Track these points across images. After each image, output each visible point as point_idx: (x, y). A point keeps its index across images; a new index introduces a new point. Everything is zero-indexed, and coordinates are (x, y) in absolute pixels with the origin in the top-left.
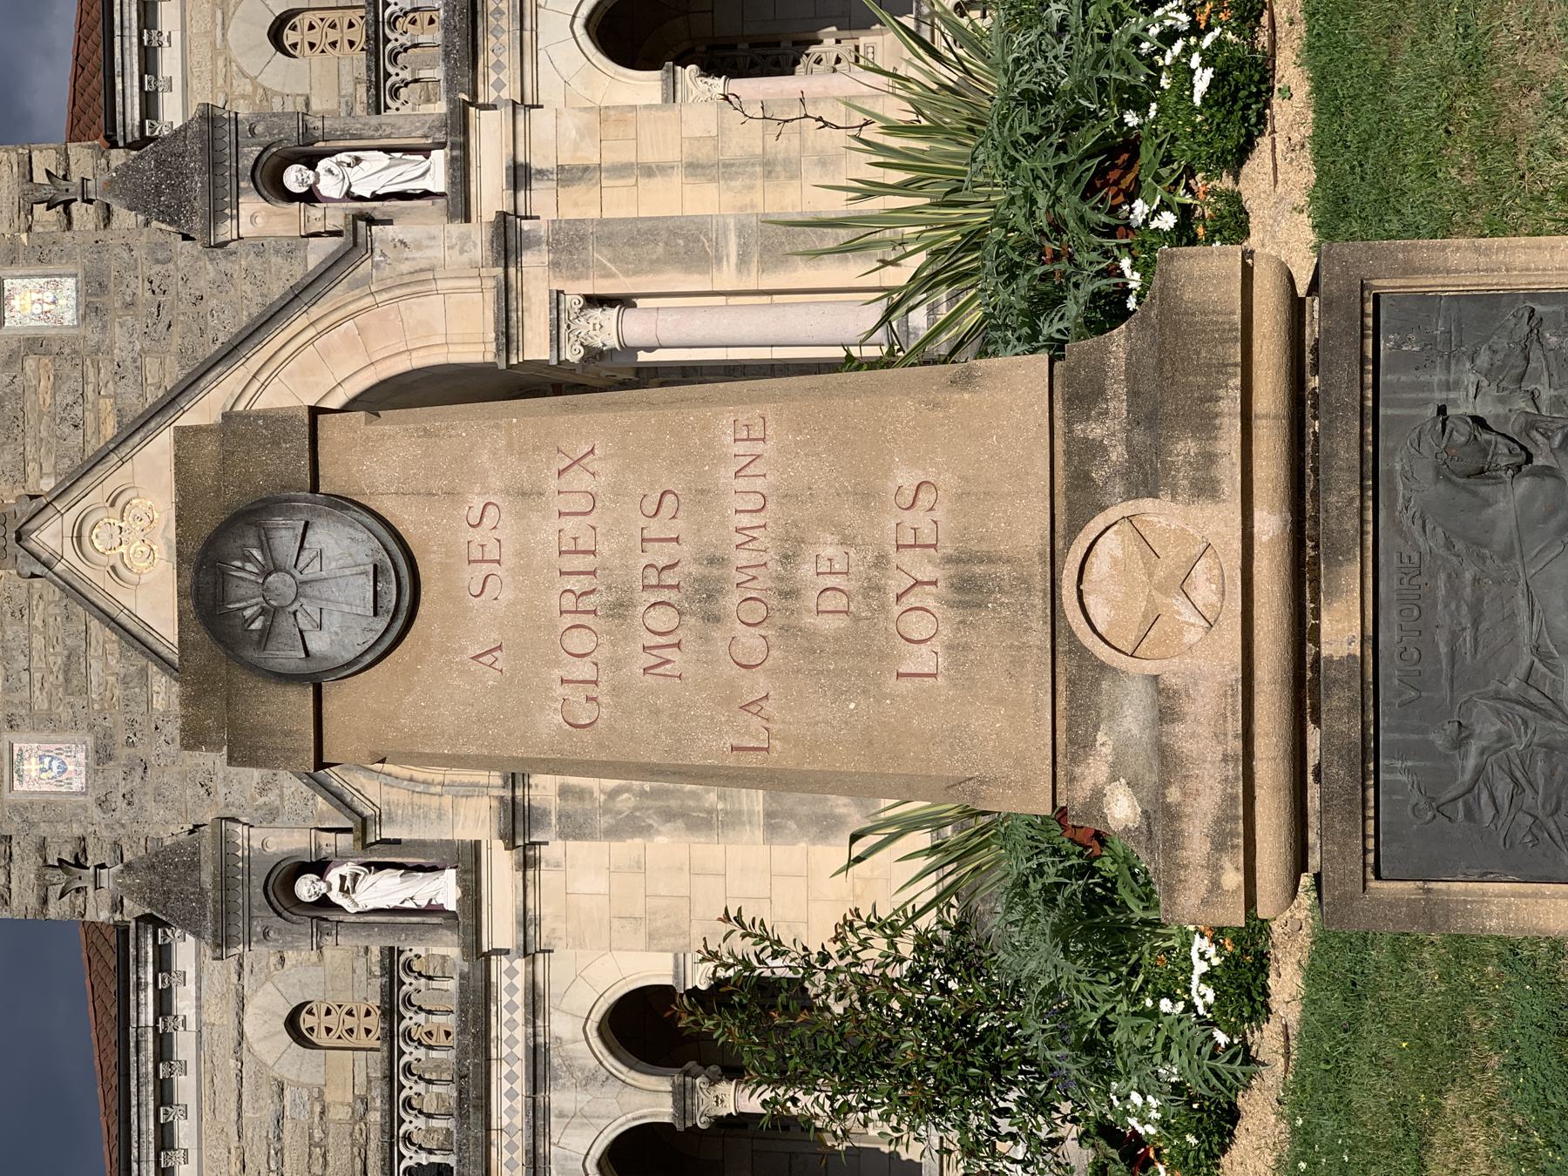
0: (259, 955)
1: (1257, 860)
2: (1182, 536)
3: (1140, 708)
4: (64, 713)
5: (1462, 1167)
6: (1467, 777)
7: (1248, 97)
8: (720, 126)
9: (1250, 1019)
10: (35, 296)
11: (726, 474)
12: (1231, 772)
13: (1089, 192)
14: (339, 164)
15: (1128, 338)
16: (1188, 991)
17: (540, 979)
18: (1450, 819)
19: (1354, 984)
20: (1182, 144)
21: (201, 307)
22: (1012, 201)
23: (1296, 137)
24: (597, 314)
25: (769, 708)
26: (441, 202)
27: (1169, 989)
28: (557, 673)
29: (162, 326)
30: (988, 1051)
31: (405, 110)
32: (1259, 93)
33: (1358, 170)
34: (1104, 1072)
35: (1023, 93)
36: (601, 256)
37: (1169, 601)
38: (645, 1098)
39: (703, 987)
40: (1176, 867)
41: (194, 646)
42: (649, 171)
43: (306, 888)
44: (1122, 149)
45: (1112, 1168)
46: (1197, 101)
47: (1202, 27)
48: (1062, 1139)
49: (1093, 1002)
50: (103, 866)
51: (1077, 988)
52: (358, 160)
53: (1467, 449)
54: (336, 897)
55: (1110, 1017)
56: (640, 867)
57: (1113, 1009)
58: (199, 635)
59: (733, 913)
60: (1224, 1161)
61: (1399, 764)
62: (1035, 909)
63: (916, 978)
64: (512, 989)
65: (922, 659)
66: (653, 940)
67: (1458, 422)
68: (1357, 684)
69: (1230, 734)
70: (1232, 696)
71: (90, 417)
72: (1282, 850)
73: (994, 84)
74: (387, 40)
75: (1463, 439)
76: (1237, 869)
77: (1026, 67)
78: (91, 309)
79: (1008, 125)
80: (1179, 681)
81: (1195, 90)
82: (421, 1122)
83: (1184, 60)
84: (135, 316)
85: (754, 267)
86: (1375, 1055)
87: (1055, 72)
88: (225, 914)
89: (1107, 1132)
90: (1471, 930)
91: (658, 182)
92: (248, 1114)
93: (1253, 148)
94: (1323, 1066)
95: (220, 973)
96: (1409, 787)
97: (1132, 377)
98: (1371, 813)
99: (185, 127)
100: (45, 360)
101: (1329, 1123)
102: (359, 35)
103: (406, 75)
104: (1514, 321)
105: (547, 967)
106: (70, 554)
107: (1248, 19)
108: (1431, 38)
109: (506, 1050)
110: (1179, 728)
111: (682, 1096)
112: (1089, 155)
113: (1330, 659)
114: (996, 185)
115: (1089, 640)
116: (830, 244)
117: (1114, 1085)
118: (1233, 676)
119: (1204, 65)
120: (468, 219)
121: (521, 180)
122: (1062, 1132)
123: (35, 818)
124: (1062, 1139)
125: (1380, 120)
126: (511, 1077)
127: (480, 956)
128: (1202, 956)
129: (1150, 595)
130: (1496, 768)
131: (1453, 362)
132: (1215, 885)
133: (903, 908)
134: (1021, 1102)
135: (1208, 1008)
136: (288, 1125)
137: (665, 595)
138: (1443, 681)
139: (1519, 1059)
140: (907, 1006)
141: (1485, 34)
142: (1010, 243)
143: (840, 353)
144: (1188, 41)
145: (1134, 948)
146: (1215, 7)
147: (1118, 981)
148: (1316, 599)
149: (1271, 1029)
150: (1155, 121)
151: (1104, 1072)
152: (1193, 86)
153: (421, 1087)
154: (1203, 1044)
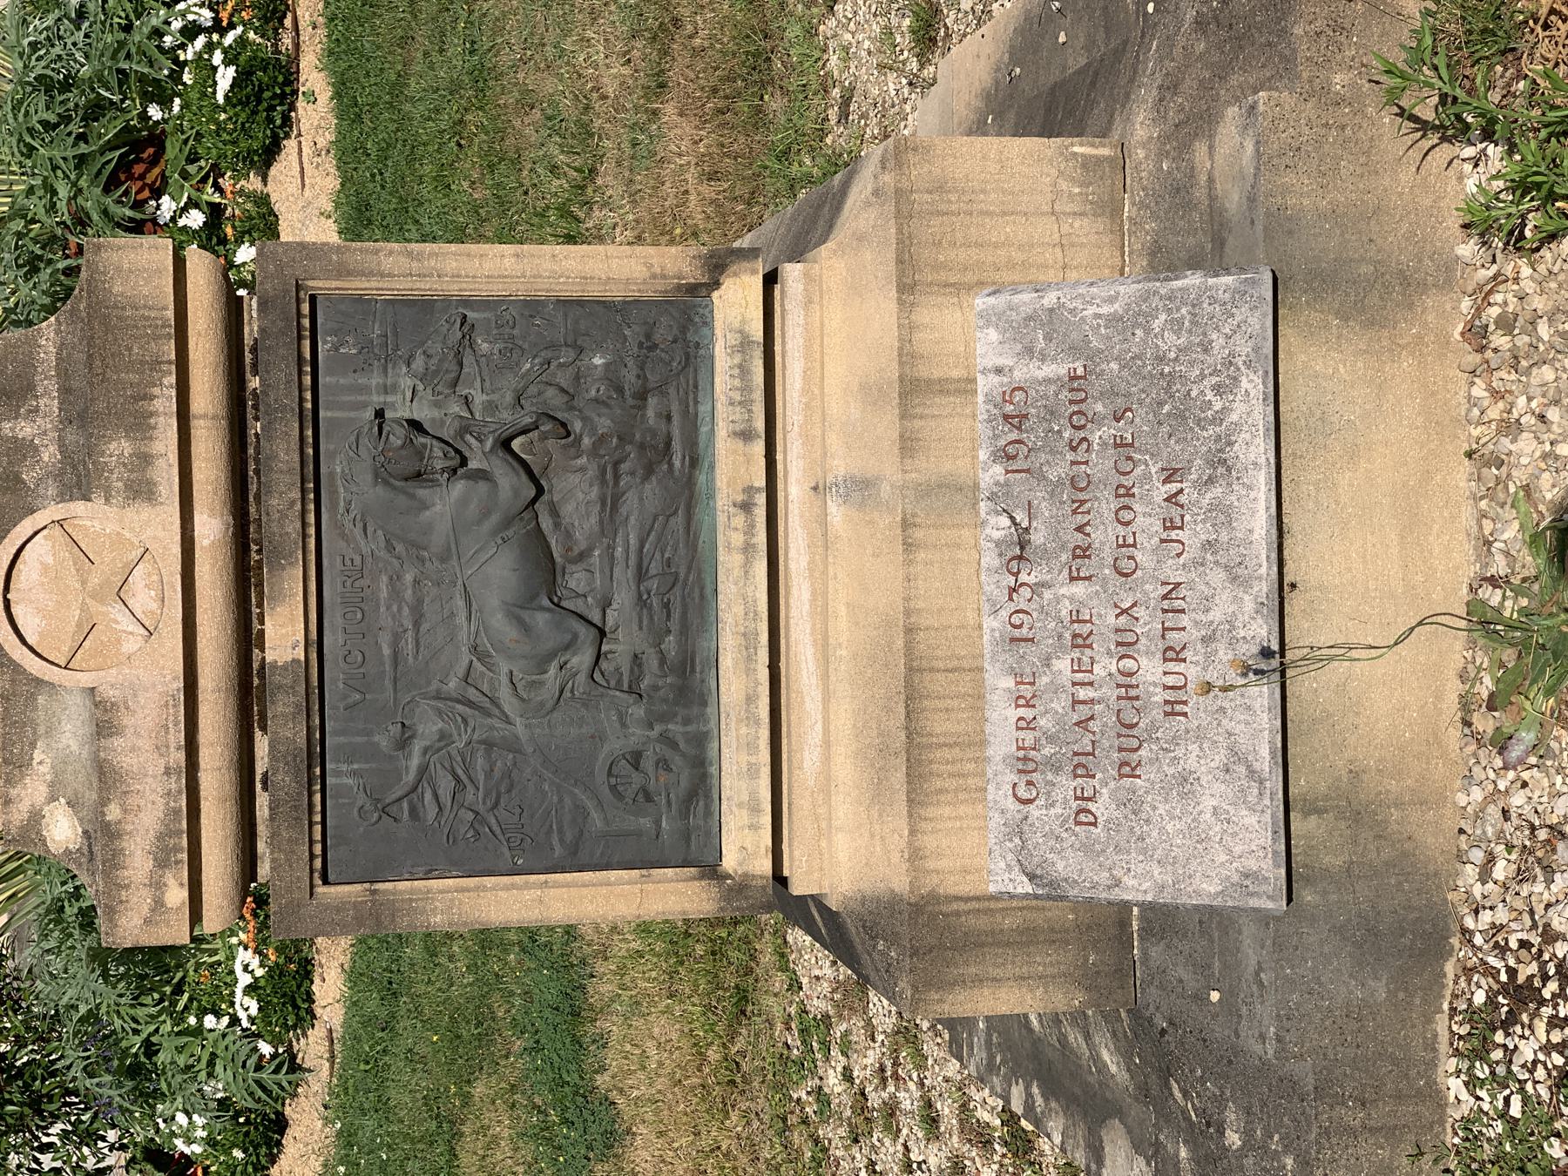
1: (204, 874)
3: (79, 723)
5: (489, 1152)
6: (410, 777)
7: (271, 98)
9: (295, 1027)
12: (174, 786)
15: (58, 332)
16: (232, 1004)
18: (395, 820)
19: (390, 983)
22: (30, 191)
23: (322, 143)
27: (214, 1004)
30: (27, 1086)
32: (283, 96)
33: (378, 178)
34: (148, 1095)
35: (39, 78)
37: (104, 609)
40: (115, 886)
46: (220, 99)
47: (224, 24)
49: (134, 1026)
51: (118, 1013)
53: (404, 452)
55: (153, 1039)
57: (157, 1030)
61: (344, 767)
62: (71, 935)
67: (394, 425)
68: (302, 689)
69: (173, 746)
70: (174, 706)
72: (229, 862)
75: (399, 442)
76: (182, 885)
77: (42, 52)
79: (23, 110)
80: (117, 693)
81: (218, 88)
83: (206, 56)
86: (410, 1050)
87: (75, 61)
90: (416, 927)
93: (280, 150)
94: (362, 1067)
96: (355, 789)
97: (63, 373)
98: (318, 818)
104: (447, 326)
107: (271, 19)
108: (441, 51)
110: (117, 742)
112: (111, 146)
113: (274, 665)
114: (13, 173)
117: (160, 1107)
118: (175, 686)
122: (108, 1162)
125: (398, 130)
128: (246, 968)
129: (83, 602)
130: (438, 766)
131: (390, 366)
132: (159, 903)
134: (65, 1135)
135: (252, 1020)
138: (387, 682)
139: (537, 1042)
141: (490, 50)
142: (32, 235)
144: (210, 38)
145: (179, 966)
146: (237, 5)
147: (161, 1001)
148: (260, 605)
150: (181, 117)
151: (148, 1095)
152: (215, 83)
154: (249, 1057)
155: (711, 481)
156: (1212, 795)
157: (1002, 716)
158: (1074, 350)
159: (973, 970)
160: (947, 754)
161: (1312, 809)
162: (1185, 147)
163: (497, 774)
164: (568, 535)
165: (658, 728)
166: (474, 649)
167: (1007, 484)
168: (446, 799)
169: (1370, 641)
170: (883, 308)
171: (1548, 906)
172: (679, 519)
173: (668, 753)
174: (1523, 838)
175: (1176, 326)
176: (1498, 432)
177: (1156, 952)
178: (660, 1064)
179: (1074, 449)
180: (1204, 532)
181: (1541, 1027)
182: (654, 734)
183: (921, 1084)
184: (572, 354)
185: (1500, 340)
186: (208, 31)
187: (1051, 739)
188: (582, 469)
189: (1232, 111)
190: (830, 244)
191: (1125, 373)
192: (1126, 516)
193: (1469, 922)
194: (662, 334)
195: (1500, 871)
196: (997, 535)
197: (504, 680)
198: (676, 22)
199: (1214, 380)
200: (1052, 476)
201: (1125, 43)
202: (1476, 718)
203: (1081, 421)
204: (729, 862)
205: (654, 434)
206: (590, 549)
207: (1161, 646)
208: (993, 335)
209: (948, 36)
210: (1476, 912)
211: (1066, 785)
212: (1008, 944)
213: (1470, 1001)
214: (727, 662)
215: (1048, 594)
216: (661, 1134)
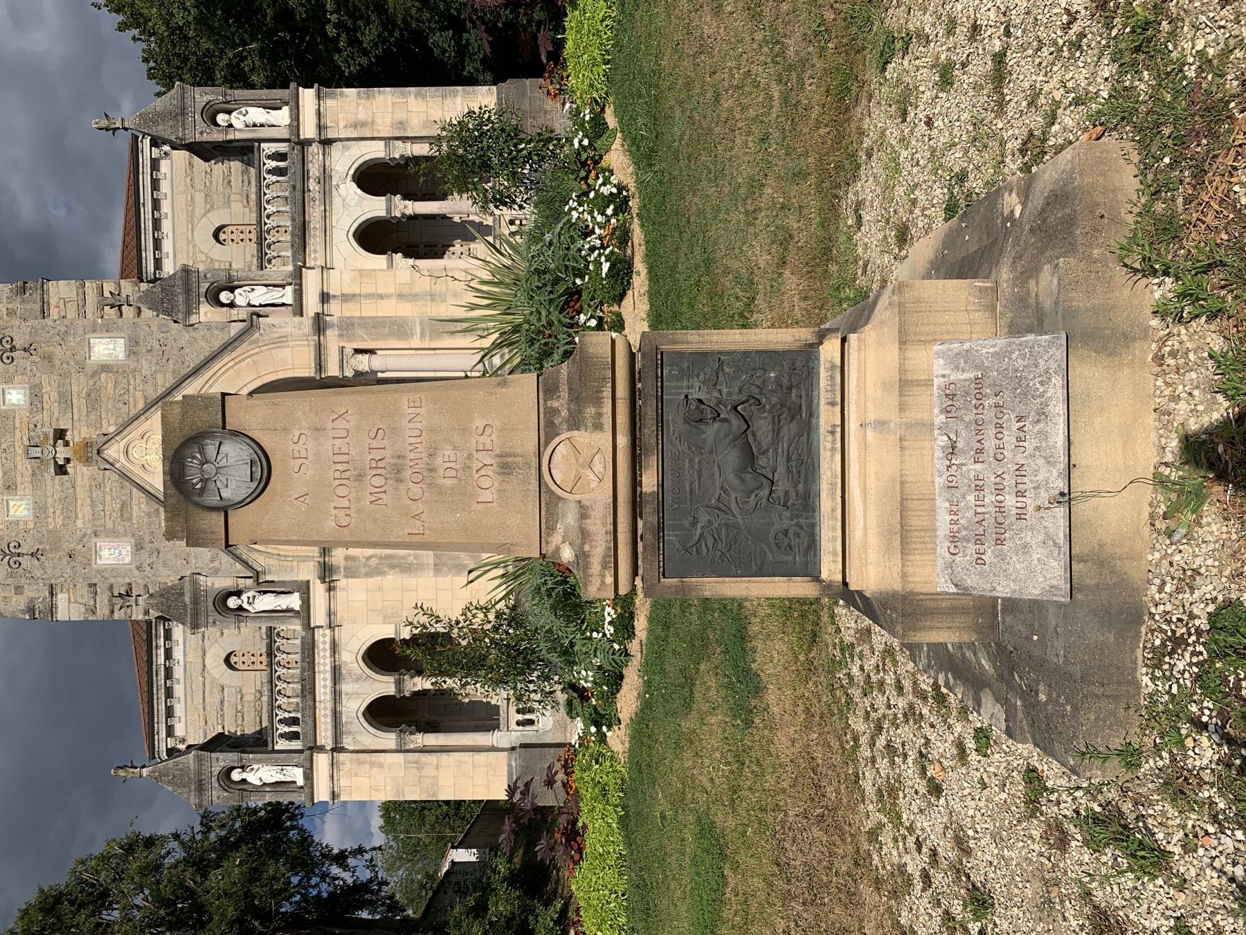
0: (212, 632)
2: (589, 446)
4: (120, 529)
8: (412, 279)
10: (105, 347)
11: (405, 422)
13: (562, 310)
17: (336, 637)
20: (598, 292)
21: (183, 351)
22: (531, 313)
23: (642, 291)
24: (360, 356)
25: (424, 517)
26: (290, 308)
28: (333, 504)
29: (164, 360)
31: (274, 269)
35: (535, 269)
36: (361, 332)
38: (382, 685)
40: (587, 575)
41: (171, 496)
42: (381, 297)
43: (232, 602)
44: (574, 294)
45: (574, 701)
46: (604, 276)
48: (555, 691)
50: (139, 596)
52: (253, 290)
54: (245, 606)
56: (380, 589)
58: (172, 491)
59: (419, 605)
60: (618, 696)
63: (496, 629)
64: (324, 642)
65: (487, 496)
66: (386, 620)
71: (131, 400)
73: (524, 265)
74: (266, 239)
78: (132, 352)
82: (285, 700)
84: (152, 356)
85: (427, 338)
88: (196, 614)
89: (573, 687)
91: (385, 301)
95: (194, 640)
97: (569, 383)
99: (175, 274)
100: (110, 375)
101: (657, 678)
102: (253, 236)
103: (275, 254)
105: (340, 632)
106: (123, 459)
109: (322, 668)
110: (588, 521)
111: (399, 684)
112: (562, 295)
113: (646, 493)
115: (554, 487)
116: (460, 329)
119: (606, 261)
120: (302, 316)
121: (325, 299)
124: (555, 691)
126: (324, 679)
127: (309, 629)
132: (603, 583)
133: (490, 601)
134: (538, 677)
135: (611, 635)
136: (226, 704)
137: (379, 471)
140: (492, 640)
143: (463, 374)
148: (640, 470)
149: (635, 642)
153: (285, 685)
155: (818, 422)
156: (1037, 553)
157: (943, 520)
158: (977, 367)
159: (928, 623)
160: (917, 534)
161: (1082, 560)
162: (1025, 282)
163: (730, 537)
164: (760, 444)
165: (795, 521)
166: (722, 488)
167: (947, 423)
168: (710, 546)
169: (1109, 489)
170: (892, 352)
171: (1191, 604)
172: (805, 436)
173: (799, 531)
174: (1179, 574)
175: (1023, 357)
176: (1169, 400)
177: (1008, 619)
178: (779, 660)
179: (977, 408)
180: (1035, 443)
181: (1187, 655)
182: (793, 523)
183: (895, 673)
184: (762, 372)
185: (1171, 361)
186: (599, 249)
187: (966, 529)
188: (765, 418)
189: (1047, 267)
190: (869, 326)
191: (1000, 377)
192: (1000, 436)
193: (1153, 610)
194: (798, 364)
195: (1168, 588)
196: (942, 444)
197: (733, 500)
198: (791, 236)
199: (1040, 379)
200: (967, 419)
201: (996, 239)
202: (1157, 523)
203: (980, 396)
204: (824, 576)
205: (795, 404)
206: (769, 449)
207: (1015, 490)
208: (941, 361)
209: (912, 238)
210: (1156, 605)
211: (972, 548)
212: (944, 614)
213: (1153, 644)
214: (823, 495)
215: (964, 468)
216: (779, 689)
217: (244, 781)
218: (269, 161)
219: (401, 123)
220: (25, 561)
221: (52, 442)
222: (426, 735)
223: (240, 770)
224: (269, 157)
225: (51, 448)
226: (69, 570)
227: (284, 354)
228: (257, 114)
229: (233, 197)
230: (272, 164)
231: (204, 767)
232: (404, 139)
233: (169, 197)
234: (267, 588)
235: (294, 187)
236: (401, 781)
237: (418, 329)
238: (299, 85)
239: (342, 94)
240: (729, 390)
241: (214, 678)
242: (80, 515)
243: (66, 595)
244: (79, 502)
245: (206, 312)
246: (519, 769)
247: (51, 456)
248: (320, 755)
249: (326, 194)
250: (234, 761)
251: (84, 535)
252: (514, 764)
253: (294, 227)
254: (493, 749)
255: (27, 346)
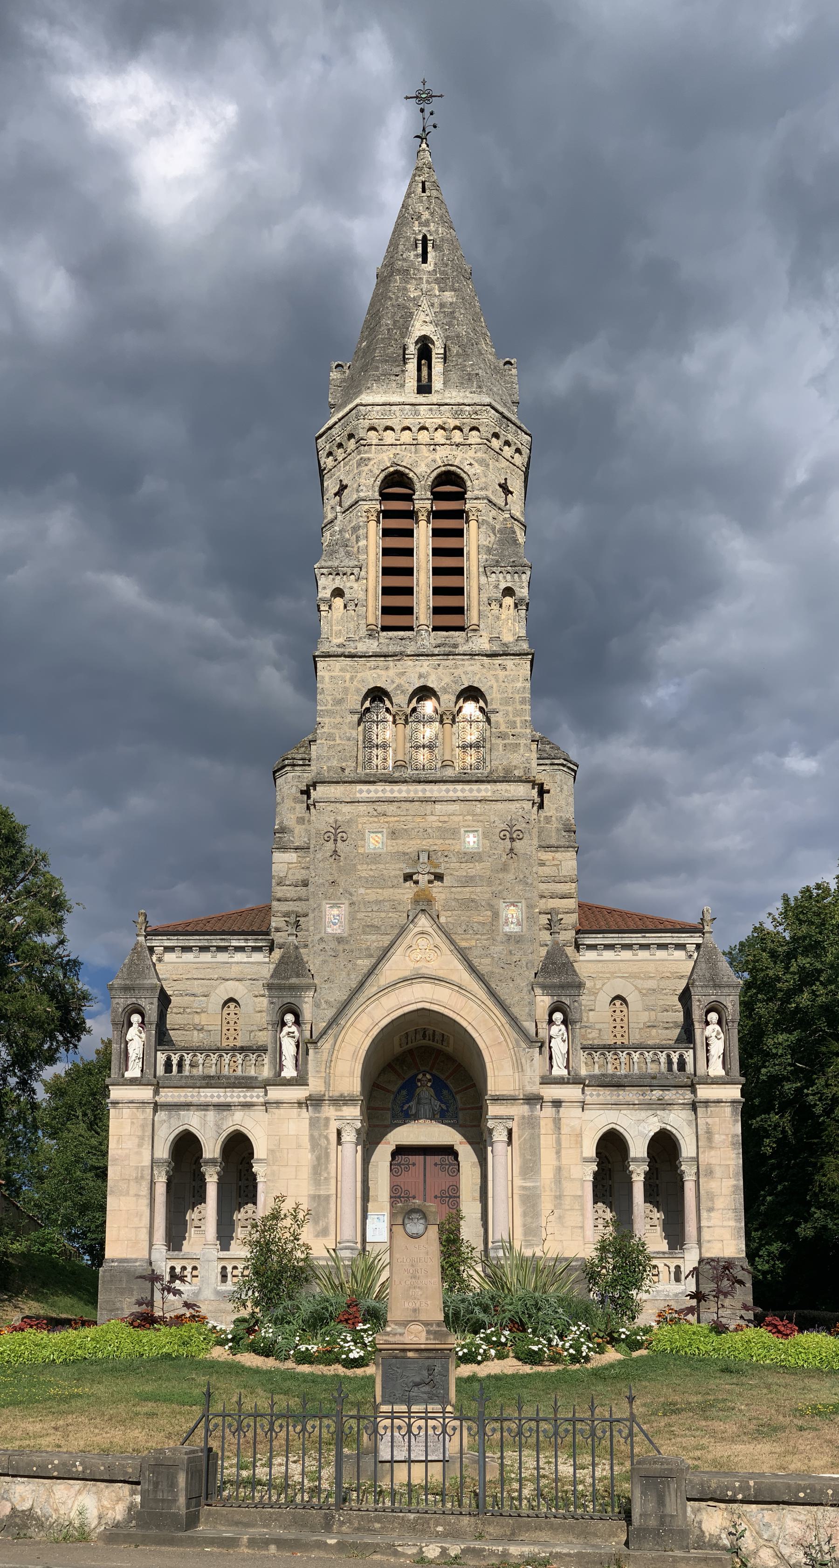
4: (355, 925)
14: (563, 1034)
17: (256, 1108)
21: (510, 981)
24: (506, 1133)
26: (548, 1073)
29: (502, 965)
36: (526, 1135)
38: (212, 1148)
39: (253, 1170)
42: (558, 1152)
52: (564, 1041)
54: (286, 1029)
56: (299, 1147)
64: (252, 1097)
65: (406, 1305)
66: (271, 1152)
71: (468, 936)
78: (509, 937)
88: (280, 988)
91: (554, 1156)
92: (196, 982)
100: (490, 919)
105: (261, 1111)
106: (416, 930)
109: (229, 1094)
111: (213, 1162)
112: (521, 1320)
123: (316, 913)
127: (265, 1085)
136: (192, 998)
149: (294, 1365)
217: (130, 1024)
218: (678, 1056)
219: (711, 1172)
220: (330, 845)
221: (432, 871)
222: (165, 1185)
223: (140, 1021)
224: (681, 1056)
225: (427, 870)
226: (321, 881)
227: (507, 1069)
228: (717, 1047)
229: (653, 1013)
230: (675, 1059)
231: (145, 992)
232: (698, 1174)
233: (652, 957)
234: (303, 1047)
235: (654, 1078)
236: (126, 1163)
237: (528, 1184)
238: (743, 1085)
239: (737, 1121)
240: (437, 1379)
241: (216, 988)
242: (369, 891)
243: (295, 861)
244: (380, 891)
245: (544, 1002)
246: (132, 1269)
247: (420, 870)
248: (152, 1091)
249: (649, 1106)
250: (149, 1017)
251: (351, 894)
252: (137, 1264)
253: (620, 1077)
254: (151, 1245)
255: (515, 851)
